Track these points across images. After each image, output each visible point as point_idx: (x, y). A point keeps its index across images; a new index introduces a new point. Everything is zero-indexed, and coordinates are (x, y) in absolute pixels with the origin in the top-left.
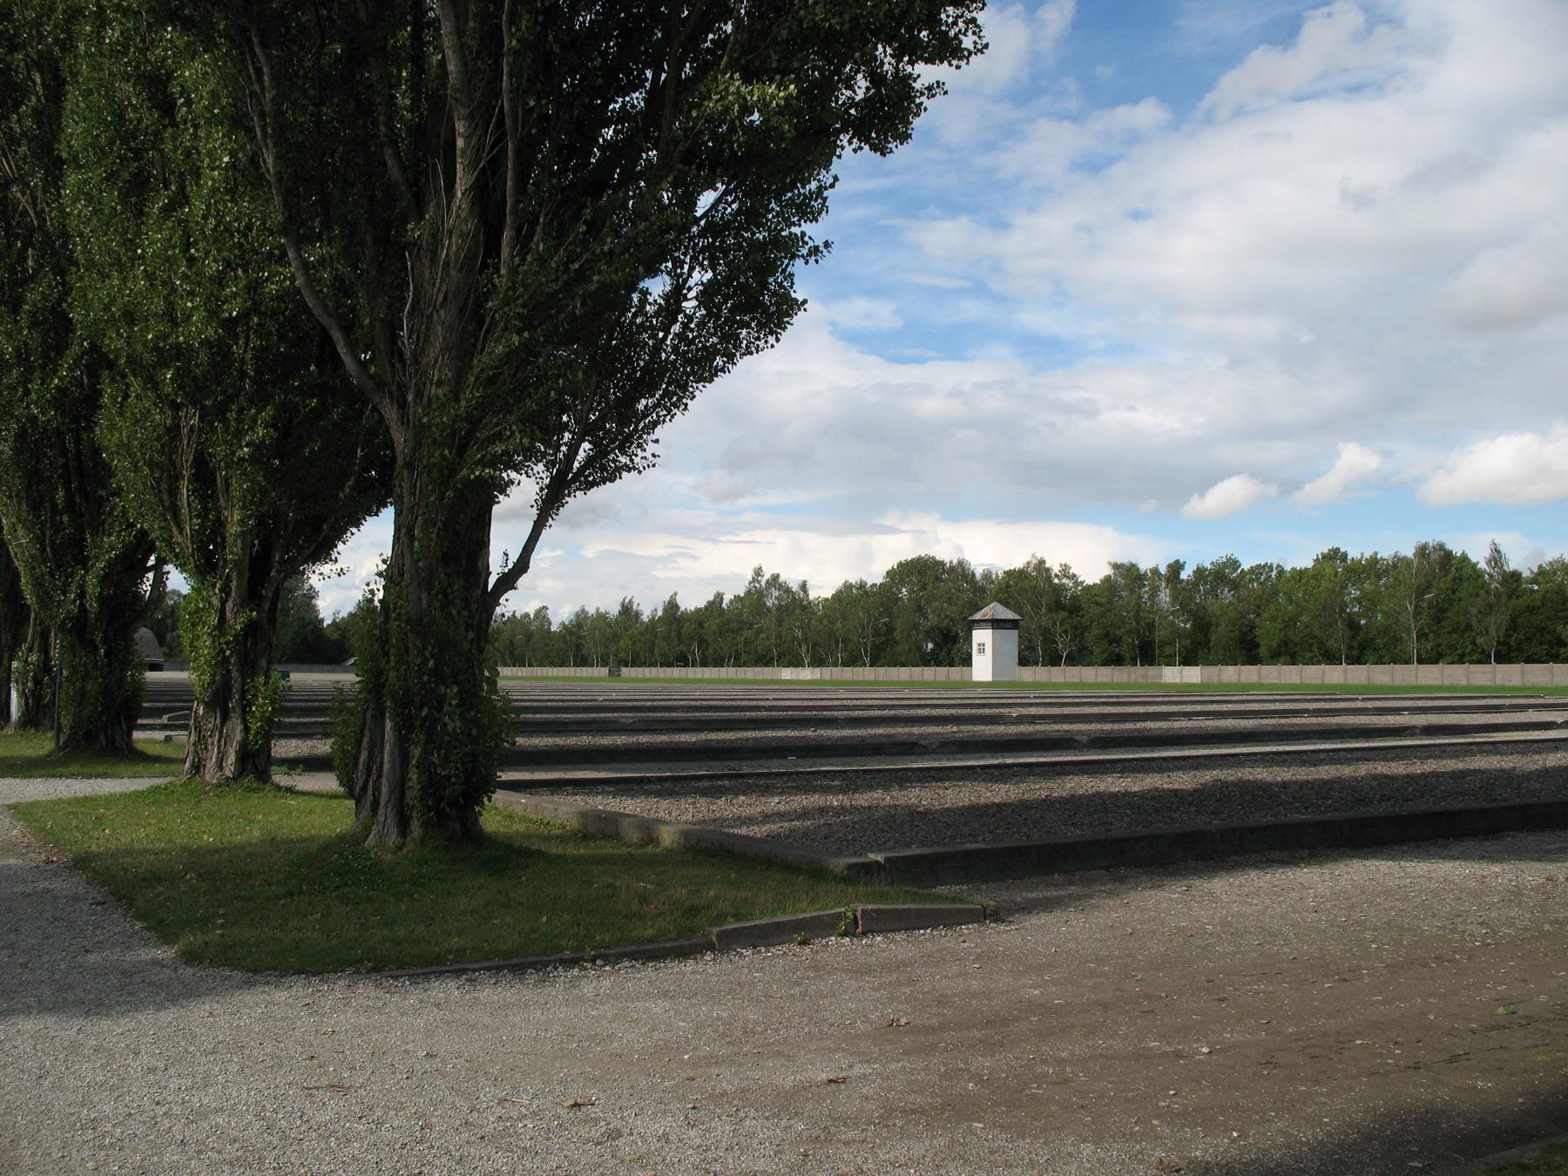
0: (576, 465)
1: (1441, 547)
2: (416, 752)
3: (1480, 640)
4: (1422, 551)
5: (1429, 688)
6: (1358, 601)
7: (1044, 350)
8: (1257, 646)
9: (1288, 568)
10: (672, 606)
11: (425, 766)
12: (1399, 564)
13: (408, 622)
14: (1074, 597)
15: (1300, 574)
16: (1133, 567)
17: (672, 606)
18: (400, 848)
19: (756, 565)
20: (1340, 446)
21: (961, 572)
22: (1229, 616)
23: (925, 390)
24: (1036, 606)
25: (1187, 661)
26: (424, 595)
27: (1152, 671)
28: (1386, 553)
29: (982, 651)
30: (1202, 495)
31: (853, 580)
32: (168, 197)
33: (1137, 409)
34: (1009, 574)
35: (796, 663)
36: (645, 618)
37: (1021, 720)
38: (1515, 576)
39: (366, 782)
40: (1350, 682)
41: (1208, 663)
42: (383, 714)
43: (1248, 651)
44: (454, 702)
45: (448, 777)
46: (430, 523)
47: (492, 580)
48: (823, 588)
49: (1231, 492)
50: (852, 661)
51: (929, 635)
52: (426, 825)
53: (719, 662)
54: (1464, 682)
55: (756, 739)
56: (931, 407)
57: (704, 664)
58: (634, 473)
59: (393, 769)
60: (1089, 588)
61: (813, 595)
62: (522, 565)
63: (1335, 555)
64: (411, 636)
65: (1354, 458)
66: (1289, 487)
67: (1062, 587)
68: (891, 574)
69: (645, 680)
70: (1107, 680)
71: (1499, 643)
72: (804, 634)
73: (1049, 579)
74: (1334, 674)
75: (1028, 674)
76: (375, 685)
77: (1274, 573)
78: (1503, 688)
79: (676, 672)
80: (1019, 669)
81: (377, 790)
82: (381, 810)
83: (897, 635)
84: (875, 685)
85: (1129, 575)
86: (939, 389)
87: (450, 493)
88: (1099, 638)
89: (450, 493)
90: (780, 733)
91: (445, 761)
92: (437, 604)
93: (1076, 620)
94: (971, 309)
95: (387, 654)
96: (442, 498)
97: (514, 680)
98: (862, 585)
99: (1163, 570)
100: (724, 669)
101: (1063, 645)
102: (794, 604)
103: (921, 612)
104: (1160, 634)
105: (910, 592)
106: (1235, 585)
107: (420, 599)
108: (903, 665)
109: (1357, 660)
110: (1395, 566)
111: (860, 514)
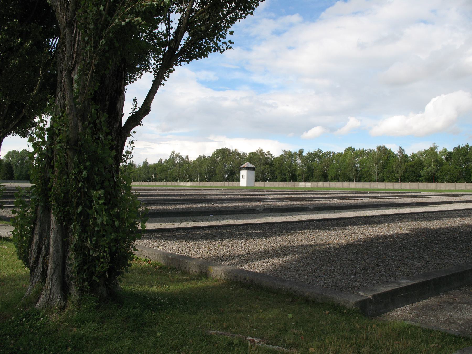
0: (182, 42)
1: (384, 147)
2: (75, 238)
3: (396, 175)
4: (379, 148)
6: (358, 163)
7: (260, 88)
8: (328, 176)
9: (336, 152)
10: (146, 163)
11: (81, 249)
12: (369, 153)
13: (68, 142)
14: (272, 161)
15: (340, 155)
16: (290, 152)
17: (146, 163)
18: (63, 309)
19: (173, 150)
20: (349, 118)
21: (236, 153)
22: (319, 167)
23: (225, 99)
24: (260, 163)
25: (307, 180)
26: (80, 124)
27: (296, 184)
28: (367, 149)
29: (243, 177)
30: (307, 132)
31: (202, 155)
32: (39, 138)
33: (288, 105)
34: (251, 154)
35: (185, 181)
36: (137, 166)
38: (406, 156)
39: (37, 258)
40: (357, 187)
41: (313, 181)
42: (49, 211)
43: (325, 178)
44: (101, 202)
45: (98, 258)
46: (87, 66)
47: (124, 120)
48: (193, 158)
49: (317, 131)
50: (202, 180)
51: (226, 172)
52: (82, 290)
53: (160, 180)
54: (392, 188)
56: (227, 104)
57: (156, 181)
58: (218, 53)
59: (56, 250)
60: (276, 158)
61: (190, 160)
62: (145, 109)
63: (351, 149)
64: (70, 154)
65: (353, 122)
66: (333, 130)
67: (268, 158)
68: (214, 154)
69: (138, 186)
70: (282, 186)
71: (401, 176)
72: (187, 172)
73: (264, 155)
74: (353, 185)
75: (258, 184)
76: (44, 190)
77: (332, 154)
78: (403, 190)
79: (147, 183)
80: (255, 183)
81: (45, 263)
82: (48, 281)
83: (217, 172)
84: (211, 188)
85: (289, 154)
86: (230, 99)
87: (103, 41)
88: (279, 174)
89: (103, 41)
90: (204, 205)
91: (96, 246)
92: (89, 131)
93: (272, 168)
94: (238, 75)
95: (52, 167)
96: (95, 47)
97: (137, 186)
98: (204, 157)
99: (298, 152)
100: (162, 182)
101: (269, 175)
102: (184, 162)
103: (224, 165)
104: (298, 173)
105: (220, 159)
106: (320, 158)
107: (77, 125)
108: (218, 181)
109: (359, 181)
110: (369, 152)
111: (203, 136)
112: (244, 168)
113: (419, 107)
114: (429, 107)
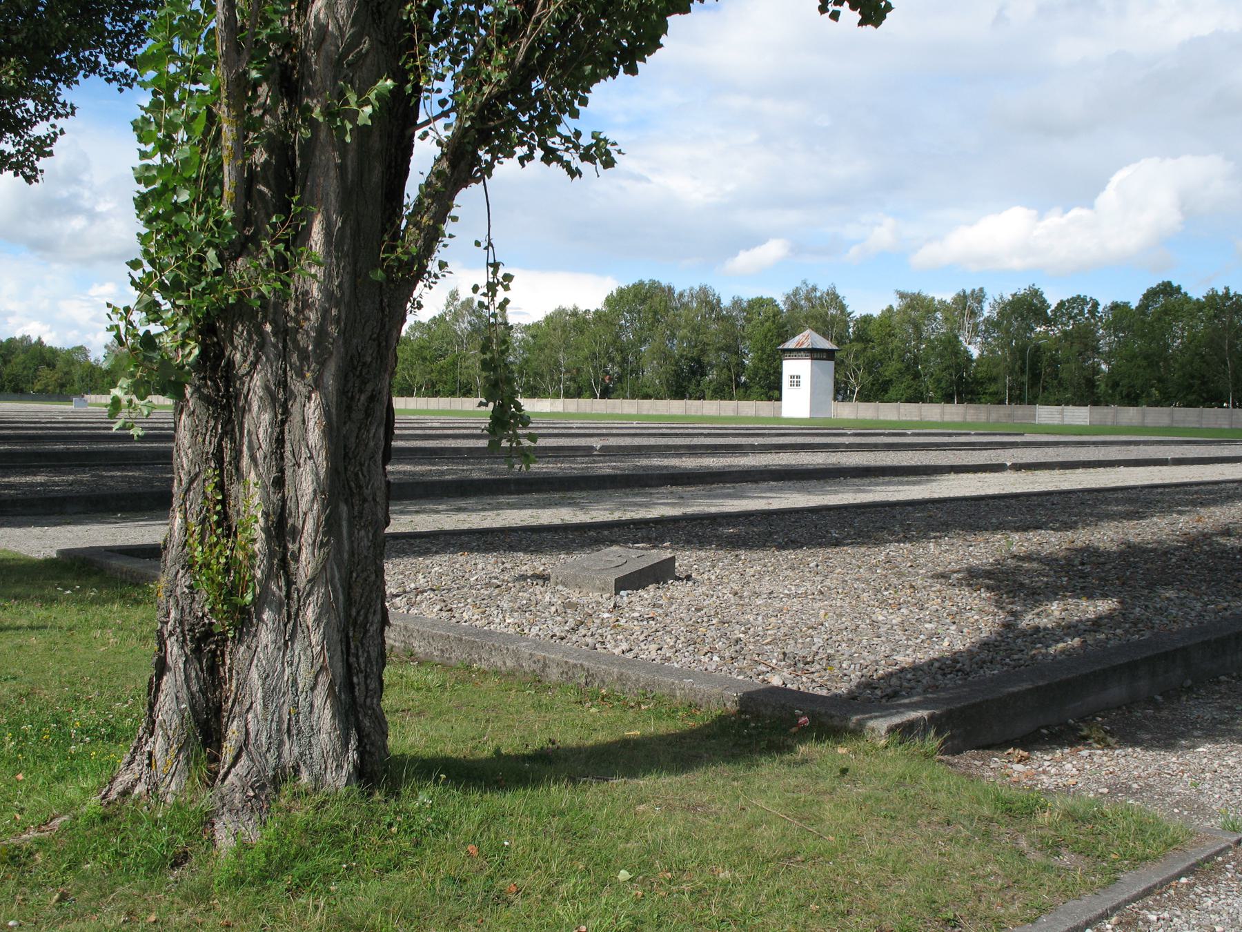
5: (890, 422)
37: (607, 452)
55: (413, 474)
75: (850, 411)
112: (797, 352)
113: (1082, 190)
114: (1109, 197)
